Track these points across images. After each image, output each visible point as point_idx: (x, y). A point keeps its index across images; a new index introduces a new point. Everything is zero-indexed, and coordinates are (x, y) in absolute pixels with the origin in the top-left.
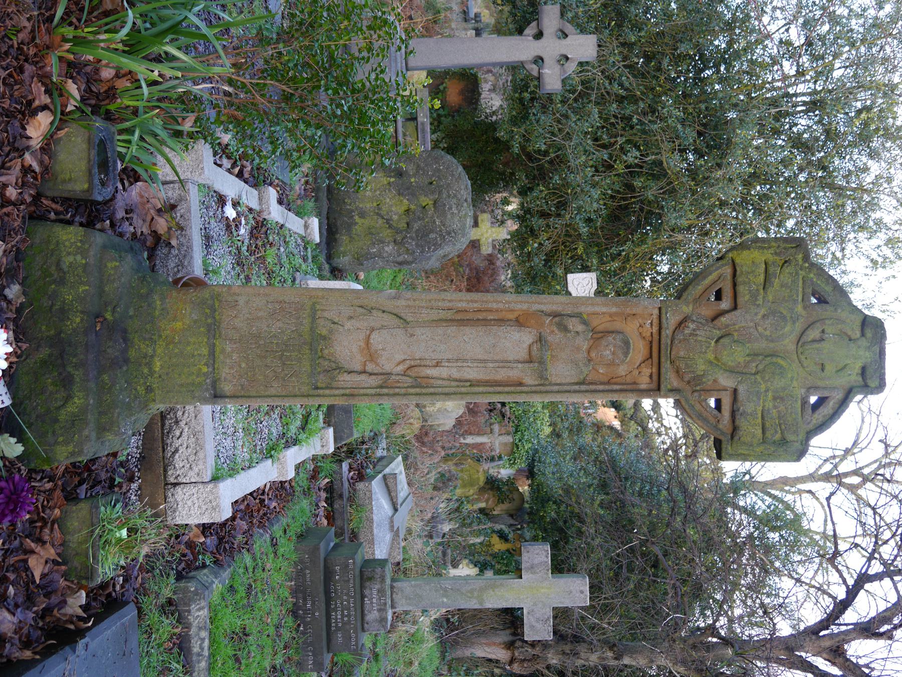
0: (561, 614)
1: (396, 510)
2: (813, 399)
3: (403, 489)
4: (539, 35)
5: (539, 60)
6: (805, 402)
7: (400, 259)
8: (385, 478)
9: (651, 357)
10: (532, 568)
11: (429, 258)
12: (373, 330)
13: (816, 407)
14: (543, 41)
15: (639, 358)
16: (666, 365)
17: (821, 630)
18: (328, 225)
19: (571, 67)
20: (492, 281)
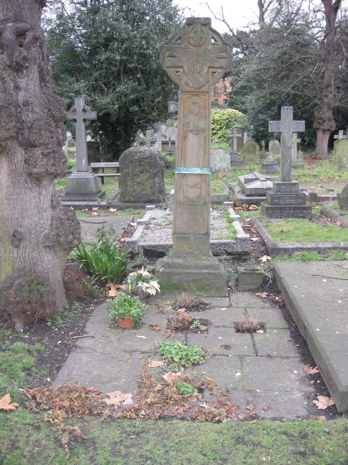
0: (296, 117)
1: (258, 179)
2: (213, 41)
3: (250, 176)
4: (75, 120)
5: (85, 120)
6: (213, 44)
7: (160, 175)
8: (246, 183)
9: (198, 95)
10: (278, 128)
11: (160, 164)
12: (187, 185)
13: (215, 40)
14: (77, 118)
15: (198, 98)
16: (201, 90)
17: (144, 340)
18: (307, 346)
19: (88, 108)
20: (228, 410)
